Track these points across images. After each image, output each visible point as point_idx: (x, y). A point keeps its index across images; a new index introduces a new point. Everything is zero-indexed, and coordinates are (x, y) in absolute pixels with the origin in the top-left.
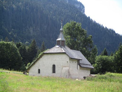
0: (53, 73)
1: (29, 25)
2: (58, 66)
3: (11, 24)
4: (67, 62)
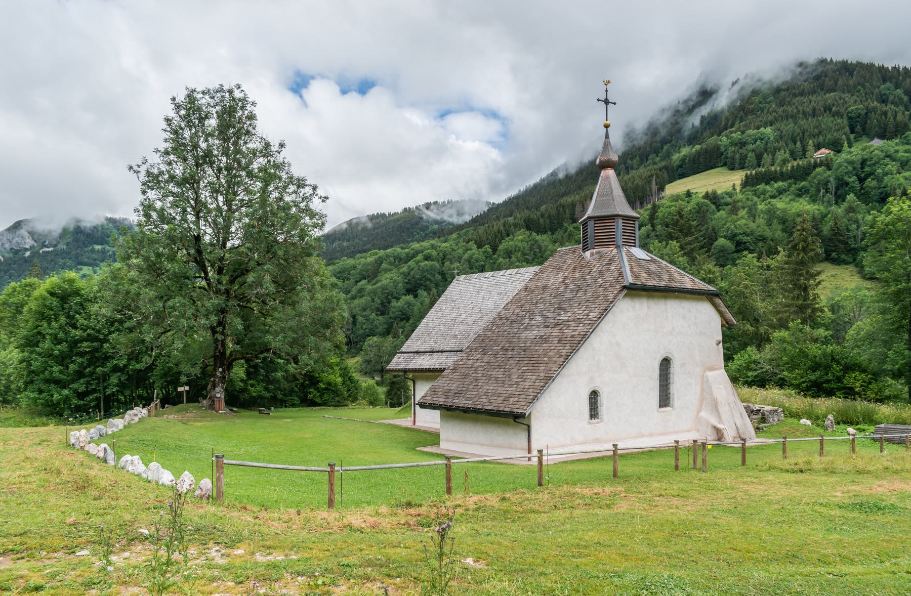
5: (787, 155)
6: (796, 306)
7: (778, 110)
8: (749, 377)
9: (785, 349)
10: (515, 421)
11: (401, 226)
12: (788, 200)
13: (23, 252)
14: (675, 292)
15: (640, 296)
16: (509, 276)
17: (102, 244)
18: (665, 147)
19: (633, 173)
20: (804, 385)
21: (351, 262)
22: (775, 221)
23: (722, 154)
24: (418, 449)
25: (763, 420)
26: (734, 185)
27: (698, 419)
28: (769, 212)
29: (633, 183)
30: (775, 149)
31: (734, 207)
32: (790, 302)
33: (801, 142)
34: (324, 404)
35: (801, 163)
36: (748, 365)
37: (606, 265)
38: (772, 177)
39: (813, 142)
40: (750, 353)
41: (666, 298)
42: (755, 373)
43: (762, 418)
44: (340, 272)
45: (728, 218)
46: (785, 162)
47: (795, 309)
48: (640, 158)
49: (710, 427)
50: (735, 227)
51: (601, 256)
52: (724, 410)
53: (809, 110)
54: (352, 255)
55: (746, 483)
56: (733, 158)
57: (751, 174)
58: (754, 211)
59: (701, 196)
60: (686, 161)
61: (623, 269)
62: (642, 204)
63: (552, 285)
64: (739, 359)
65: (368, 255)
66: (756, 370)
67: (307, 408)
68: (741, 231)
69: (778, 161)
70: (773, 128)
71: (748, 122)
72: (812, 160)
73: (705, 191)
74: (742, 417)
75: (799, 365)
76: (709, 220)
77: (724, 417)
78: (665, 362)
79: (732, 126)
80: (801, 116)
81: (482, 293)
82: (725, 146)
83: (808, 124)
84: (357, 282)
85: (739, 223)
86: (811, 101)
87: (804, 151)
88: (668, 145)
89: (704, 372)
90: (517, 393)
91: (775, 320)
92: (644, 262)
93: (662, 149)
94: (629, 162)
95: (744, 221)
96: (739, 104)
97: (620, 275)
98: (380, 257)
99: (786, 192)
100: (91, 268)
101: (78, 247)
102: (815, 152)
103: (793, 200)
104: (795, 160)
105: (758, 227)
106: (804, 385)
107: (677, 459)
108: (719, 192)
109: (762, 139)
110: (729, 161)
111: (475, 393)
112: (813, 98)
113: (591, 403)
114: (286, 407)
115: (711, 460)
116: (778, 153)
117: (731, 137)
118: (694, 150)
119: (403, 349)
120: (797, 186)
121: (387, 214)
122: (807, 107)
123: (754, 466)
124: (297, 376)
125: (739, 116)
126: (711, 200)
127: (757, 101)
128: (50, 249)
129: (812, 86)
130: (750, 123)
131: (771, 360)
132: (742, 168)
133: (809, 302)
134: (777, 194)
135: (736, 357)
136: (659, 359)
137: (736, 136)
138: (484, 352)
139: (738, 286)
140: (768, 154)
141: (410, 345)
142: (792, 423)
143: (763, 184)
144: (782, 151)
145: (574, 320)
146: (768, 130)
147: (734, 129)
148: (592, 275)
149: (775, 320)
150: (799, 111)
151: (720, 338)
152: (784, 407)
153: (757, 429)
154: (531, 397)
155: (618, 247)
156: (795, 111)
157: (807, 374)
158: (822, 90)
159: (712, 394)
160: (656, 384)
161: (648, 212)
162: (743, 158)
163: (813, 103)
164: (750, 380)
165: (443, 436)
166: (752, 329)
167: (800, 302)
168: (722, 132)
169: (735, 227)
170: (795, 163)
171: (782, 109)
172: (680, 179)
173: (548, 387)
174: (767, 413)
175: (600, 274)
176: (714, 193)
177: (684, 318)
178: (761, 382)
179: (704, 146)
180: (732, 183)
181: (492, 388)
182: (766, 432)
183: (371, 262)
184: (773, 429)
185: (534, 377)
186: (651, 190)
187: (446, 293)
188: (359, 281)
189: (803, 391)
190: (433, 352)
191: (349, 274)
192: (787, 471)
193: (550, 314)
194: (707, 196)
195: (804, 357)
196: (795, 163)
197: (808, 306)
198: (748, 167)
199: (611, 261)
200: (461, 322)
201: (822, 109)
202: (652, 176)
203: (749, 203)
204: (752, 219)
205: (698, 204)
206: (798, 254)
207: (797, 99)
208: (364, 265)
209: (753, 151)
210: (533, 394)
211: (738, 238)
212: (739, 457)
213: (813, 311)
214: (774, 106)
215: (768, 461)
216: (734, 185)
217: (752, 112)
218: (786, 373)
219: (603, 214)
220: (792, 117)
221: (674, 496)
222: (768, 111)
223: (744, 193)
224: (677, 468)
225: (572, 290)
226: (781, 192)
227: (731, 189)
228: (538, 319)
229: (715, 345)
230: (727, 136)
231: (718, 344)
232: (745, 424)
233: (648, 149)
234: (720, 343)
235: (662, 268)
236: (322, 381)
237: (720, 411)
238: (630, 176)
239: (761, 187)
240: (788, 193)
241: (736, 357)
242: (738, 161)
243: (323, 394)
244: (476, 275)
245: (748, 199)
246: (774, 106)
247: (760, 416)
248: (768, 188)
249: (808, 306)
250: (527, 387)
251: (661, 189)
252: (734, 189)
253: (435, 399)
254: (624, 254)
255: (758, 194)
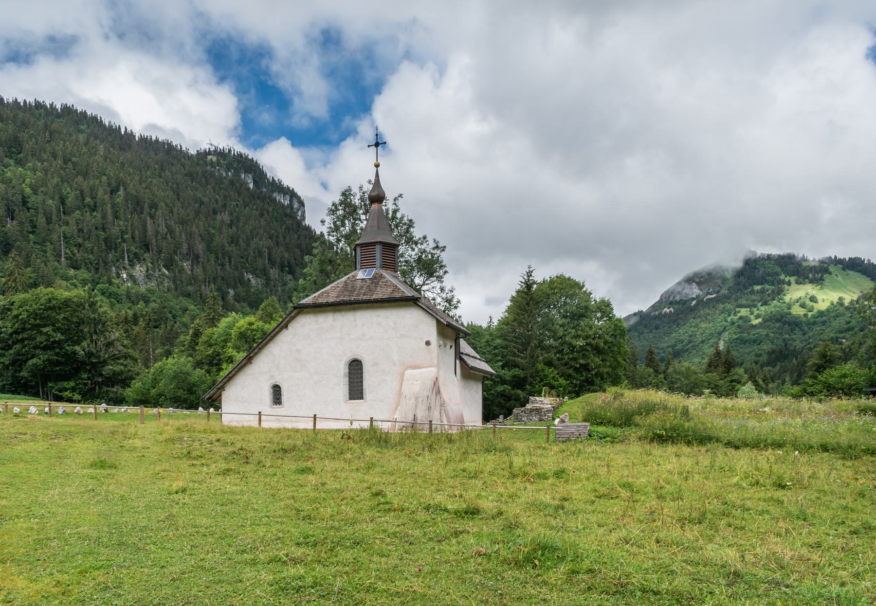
0: (351, 399)
1: (128, 257)
2: (376, 364)
3: (66, 253)
4: (428, 343)
13: (690, 301)
17: (762, 284)
100: (748, 309)
101: (739, 290)
128: (713, 296)
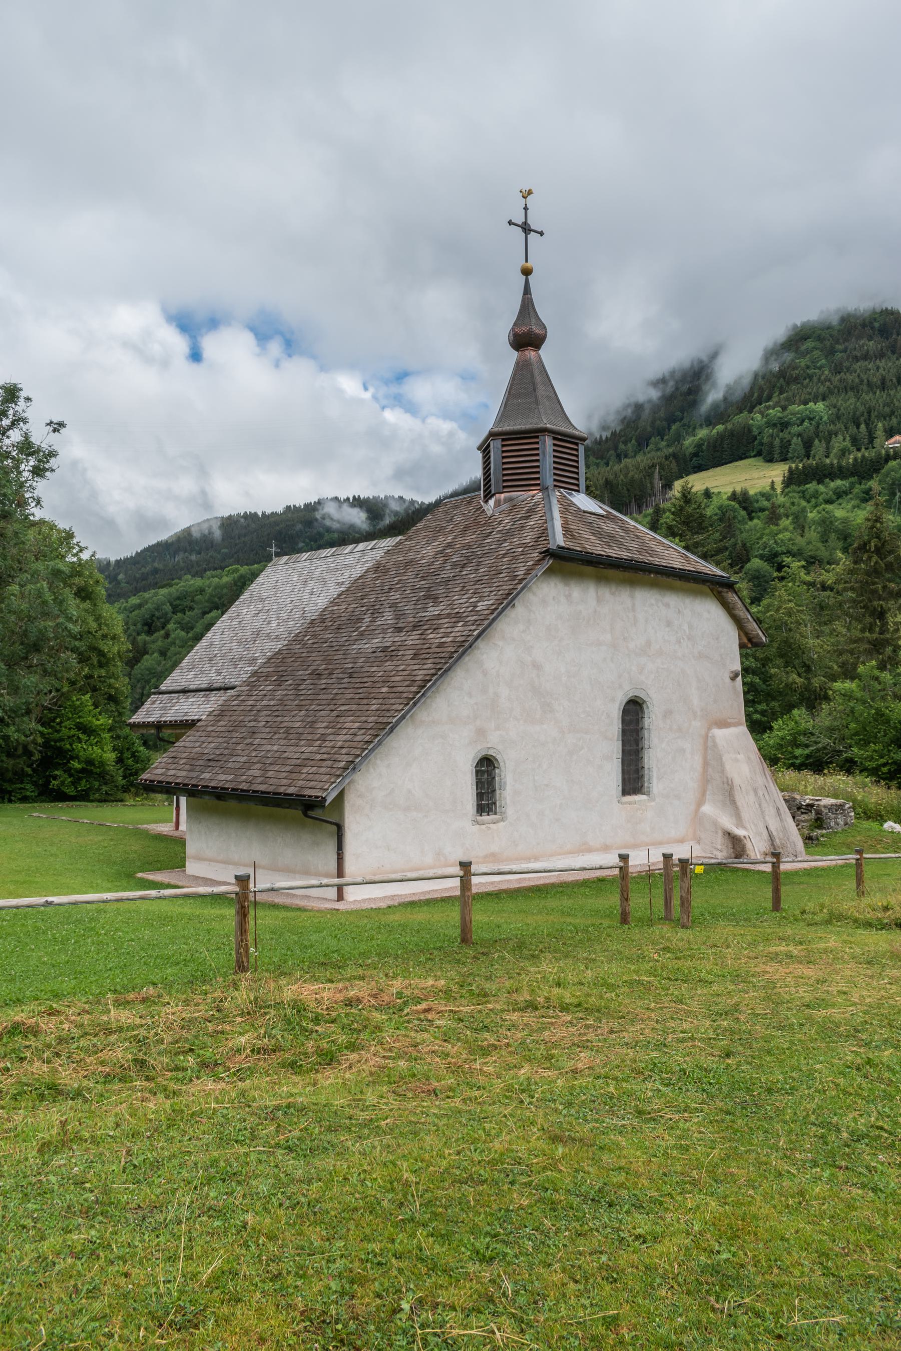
5: (848, 443)
6: (869, 642)
7: (833, 379)
8: (796, 758)
9: (852, 711)
10: (306, 815)
11: (280, 533)
12: (850, 506)
14: (650, 572)
15: (580, 576)
16: (360, 554)
18: (674, 427)
19: (626, 461)
20: (885, 770)
21: (198, 582)
22: (833, 536)
23: (755, 438)
24: (140, 875)
25: (819, 822)
26: (773, 482)
27: (697, 819)
28: (823, 522)
29: (626, 475)
30: (830, 434)
31: (773, 513)
32: (859, 634)
33: (867, 425)
34: (83, 797)
35: (867, 454)
36: (795, 738)
37: (520, 519)
38: (826, 472)
39: (884, 426)
40: (798, 718)
41: (632, 583)
42: (807, 751)
43: (817, 820)
44: (178, 598)
45: (764, 529)
46: (844, 452)
47: (867, 646)
48: (636, 441)
49: (720, 833)
50: (776, 542)
51: (514, 506)
52: (746, 801)
53: (876, 380)
54: (200, 574)
55: (774, 957)
56: (771, 445)
57: (797, 467)
58: (802, 520)
59: (725, 497)
60: (704, 447)
61: (549, 525)
62: (639, 507)
63: (423, 558)
64: (781, 729)
65: (225, 573)
66: (807, 746)
67: (46, 805)
68: (784, 549)
69: (835, 451)
70: (826, 403)
71: (790, 394)
72: (883, 452)
73: (731, 490)
74: (779, 815)
75: (876, 737)
76: (738, 532)
77: (746, 815)
78: (632, 707)
79: (769, 398)
80: (865, 387)
81: (311, 584)
82: (759, 427)
83: (876, 399)
84: (204, 613)
85: (780, 536)
86: (878, 368)
87: (872, 439)
88: (678, 423)
89: (709, 729)
90: (319, 757)
91: (836, 667)
92: (593, 517)
93: (669, 429)
94: (622, 446)
95: (787, 535)
96: (777, 369)
97: (544, 533)
98: (242, 576)
99: (847, 495)
102: (887, 440)
103: (858, 507)
104: (859, 450)
105: (809, 543)
106: (885, 770)
107: (625, 899)
108: (752, 492)
109: (811, 419)
110: (765, 449)
111: (243, 759)
112: (882, 363)
113: (479, 783)
114: (10, 801)
115: (697, 902)
116: (834, 439)
117: (767, 415)
118: (715, 431)
119: (163, 687)
120: (863, 487)
121: (260, 514)
122: (874, 375)
123: (797, 912)
124: (31, 747)
125: (778, 385)
126: (739, 503)
127: (803, 364)
129: (879, 346)
130: (794, 396)
131: (831, 730)
132: (784, 460)
133: (888, 636)
134: (834, 497)
135: (775, 725)
136: (621, 699)
137: (775, 413)
138: (279, 683)
139: (777, 610)
140: (820, 441)
141: (175, 680)
142: (870, 830)
143: (815, 483)
144: (840, 437)
145: (448, 616)
146: (820, 406)
147: (771, 403)
148: (496, 536)
149: (836, 667)
150: (862, 381)
151: (738, 667)
152: (854, 801)
153: (808, 840)
154: (342, 764)
155: (544, 489)
156: (857, 380)
157: (889, 751)
158: (893, 352)
159: (723, 771)
160: (614, 748)
161: (649, 518)
162: (786, 446)
163: (881, 371)
164: (798, 762)
165: (191, 849)
166: (799, 680)
167: (875, 636)
168: (754, 407)
169: (776, 542)
170: (859, 455)
171: (838, 377)
172: (695, 472)
173: (380, 743)
174: (825, 811)
175: (508, 534)
176: (745, 493)
177: (669, 624)
178: (817, 765)
179: (729, 426)
180: (770, 480)
181: (275, 748)
182: (824, 845)
183: (227, 582)
184: (836, 840)
185: (357, 725)
186: (652, 488)
187: (253, 586)
188: (210, 611)
189: (884, 779)
190: (210, 689)
191: (192, 601)
192: (868, 925)
193: (409, 609)
194: (734, 496)
195: (883, 723)
196: (859, 455)
197: (887, 642)
198: (792, 458)
199: (531, 511)
200: (268, 635)
201: (894, 379)
202: (654, 466)
203: (795, 509)
204: (799, 531)
205: (720, 508)
206: (870, 558)
207: (859, 364)
208: (216, 588)
209: (799, 435)
210: (346, 758)
211: (779, 559)
212: (768, 892)
213: (894, 651)
214: (826, 372)
215: (827, 903)
216: (773, 482)
217: (796, 380)
218: (855, 750)
219: (517, 427)
220: (852, 389)
221: (565, 1008)
222: (819, 379)
223: (787, 494)
224: (625, 918)
225: (454, 565)
226: (840, 495)
227: (768, 488)
228: (388, 617)
229: (728, 680)
230: (762, 413)
231: (733, 679)
232: (785, 829)
233: (649, 429)
234: (736, 676)
235: (627, 531)
236: (77, 757)
237: (739, 804)
238: (622, 465)
239: (812, 486)
240: (850, 496)
241: (775, 725)
242: (777, 450)
243: (80, 779)
244: (306, 555)
245: (793, 504)
246: (826, 372)
247: (813, 815)
248: (821, 488)
249: (887, 642)
250: (340, 744)
251: (668, 486)
252: (773, 487)
253: (172, 772)
254: (554, 502)
255: (808, 497)
